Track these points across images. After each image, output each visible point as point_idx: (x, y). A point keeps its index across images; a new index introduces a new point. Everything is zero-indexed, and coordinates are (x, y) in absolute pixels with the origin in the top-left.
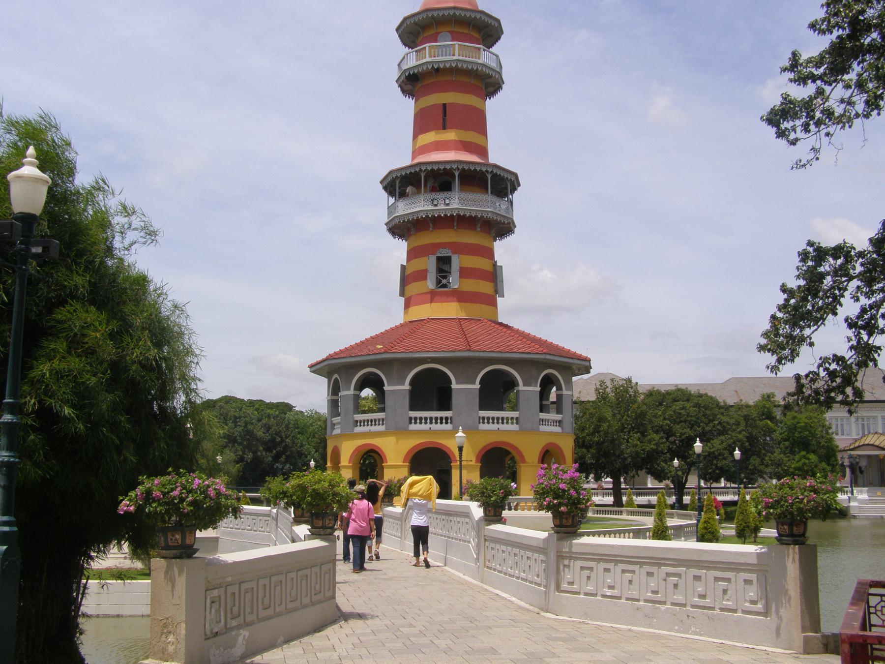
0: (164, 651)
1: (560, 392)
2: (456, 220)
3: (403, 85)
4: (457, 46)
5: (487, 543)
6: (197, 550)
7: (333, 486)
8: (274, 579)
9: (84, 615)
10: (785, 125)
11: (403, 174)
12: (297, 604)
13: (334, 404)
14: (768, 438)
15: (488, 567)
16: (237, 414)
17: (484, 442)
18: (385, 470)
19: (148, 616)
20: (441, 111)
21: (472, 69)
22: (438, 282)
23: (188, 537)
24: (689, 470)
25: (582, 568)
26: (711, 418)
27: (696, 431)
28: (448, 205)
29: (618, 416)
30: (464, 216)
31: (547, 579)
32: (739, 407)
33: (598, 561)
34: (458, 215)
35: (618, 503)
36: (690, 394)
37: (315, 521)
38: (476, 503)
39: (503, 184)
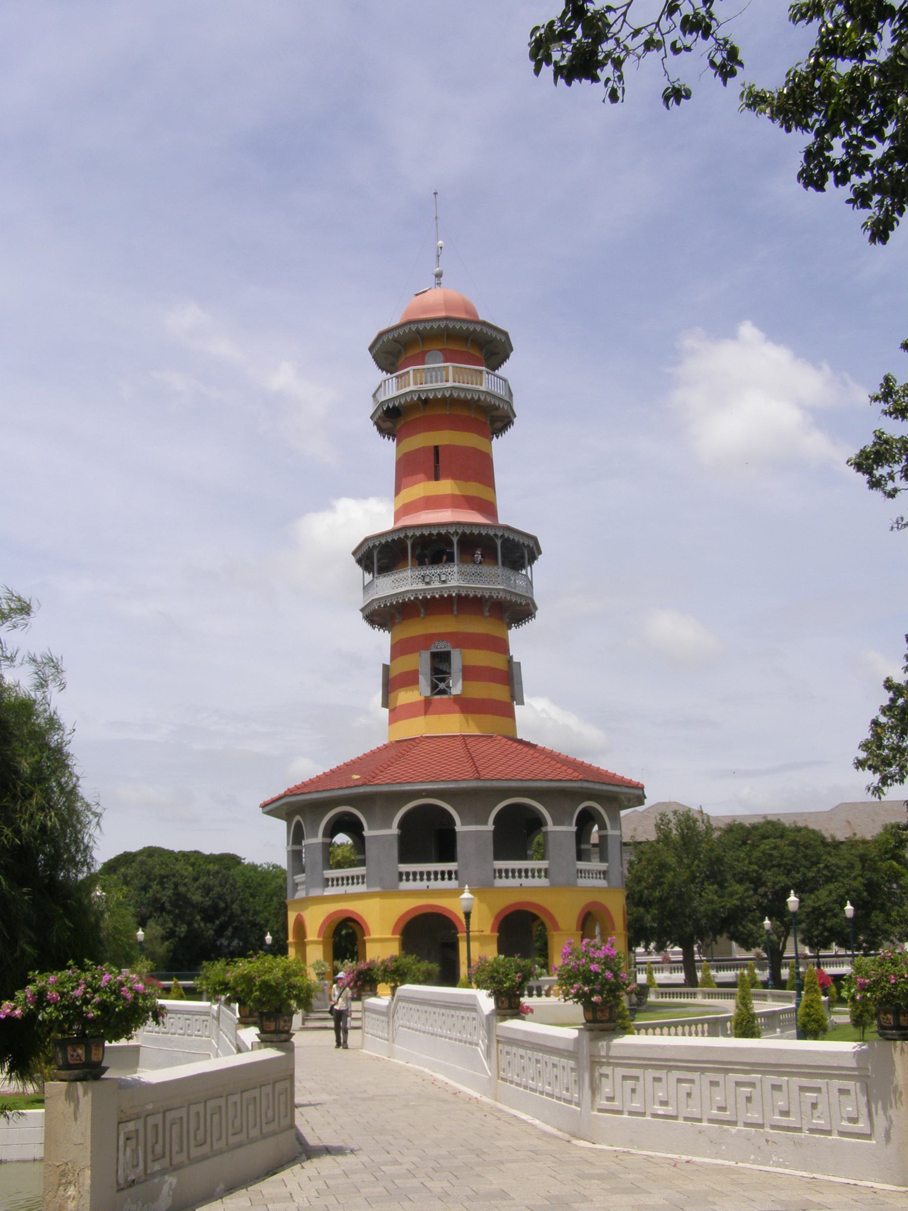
1: (603, 832)
2: (455, 603)
3: (380, 422)
4: (451, 369)
5: (501, 1046)
6: (106, 1069)
7: (289, 976)
10: (881, 471)
11: (383, 541)
12: (242, 1137)
13: (296, 856)
14: (895, 886)
15: (503, 1079)
16: (163, 872)
17: (504, 902)
18: (368, 946)
19: (41, 1160)
20: (432, 456)
21: (473, 398)
22: (434, 687)
23: (94, 1052)
25: (625, 1078)
26: (814, 859)
27: (793, 878)
28: (444, 582)
30: (467, 596)
32: (852, 843)
34: (459, 596)
35: (691, 981)
38: (485, 992)
39: (519, 551)
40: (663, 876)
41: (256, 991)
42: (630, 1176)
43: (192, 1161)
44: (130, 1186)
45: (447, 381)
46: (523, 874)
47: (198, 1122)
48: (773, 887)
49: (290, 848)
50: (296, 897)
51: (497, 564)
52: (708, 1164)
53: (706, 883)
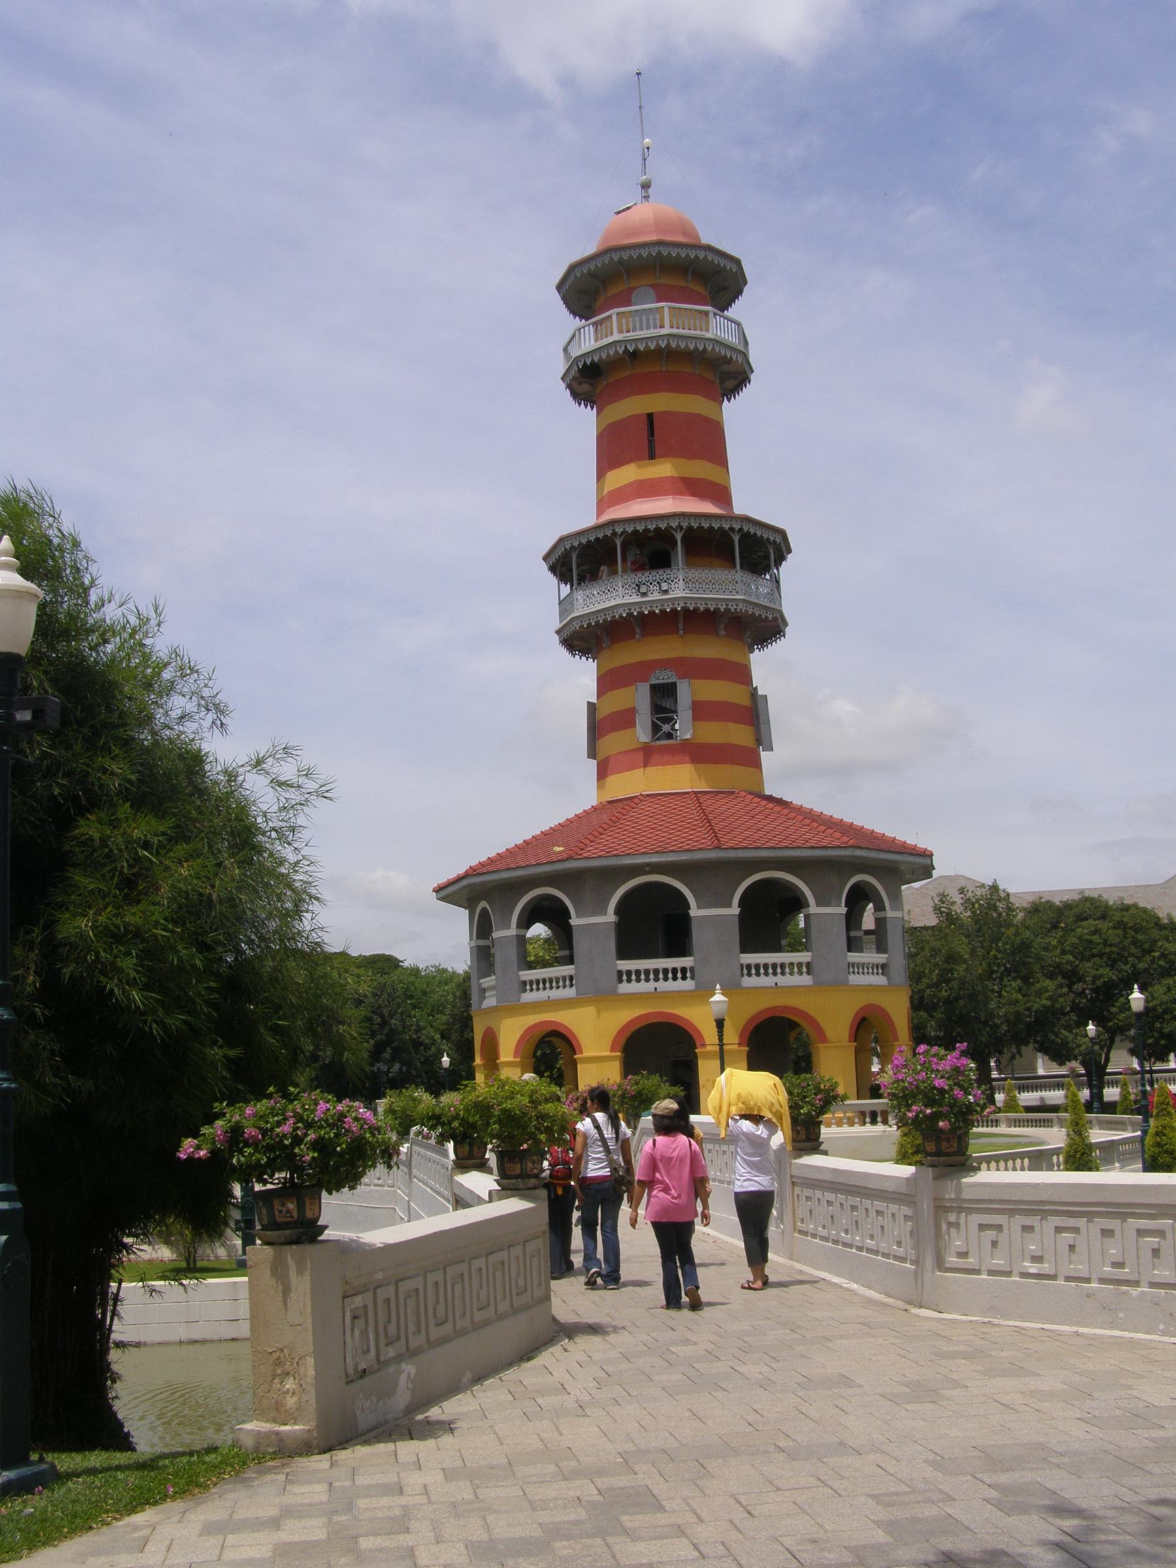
0: (278, 1405)
1: (881, 914)
2: (681, 619)
3: (575, 384)
4: (666, 311)
5: (797, 1190)
6: (325, 1227)
8: (450, 1271)
9: (120, 1345)
11: (584, 541)
13: (484, 956)
15: (800, 1232)
17: (752, 1008)
21: (696, 349)
22: (656, 728)
24: (1112, 1041)
25: (982, 1227)
26: (1147, 946)
27: (1120, 971)
28: (666, 592)
29: (980, 952)
30: (696, 610)
31: (917, 1246)
33: (1011, 1212)
34: (686, 610)
36: (1107, 906)
37: (507, 1165)
39: (761, 550)
40: (951, 971)
41: (495, 1123)
42: (1004, 1354)
43: (432, 1345)
44: (362, 1377)
45: (662, 327)
46: (779, 970)
47: (437, 1295)
48: (1093, 982)
49: (474, 944)
50: (483, 1007)
51: (734, 567)
52: (1102, 1336)
53: (1005, 979)
